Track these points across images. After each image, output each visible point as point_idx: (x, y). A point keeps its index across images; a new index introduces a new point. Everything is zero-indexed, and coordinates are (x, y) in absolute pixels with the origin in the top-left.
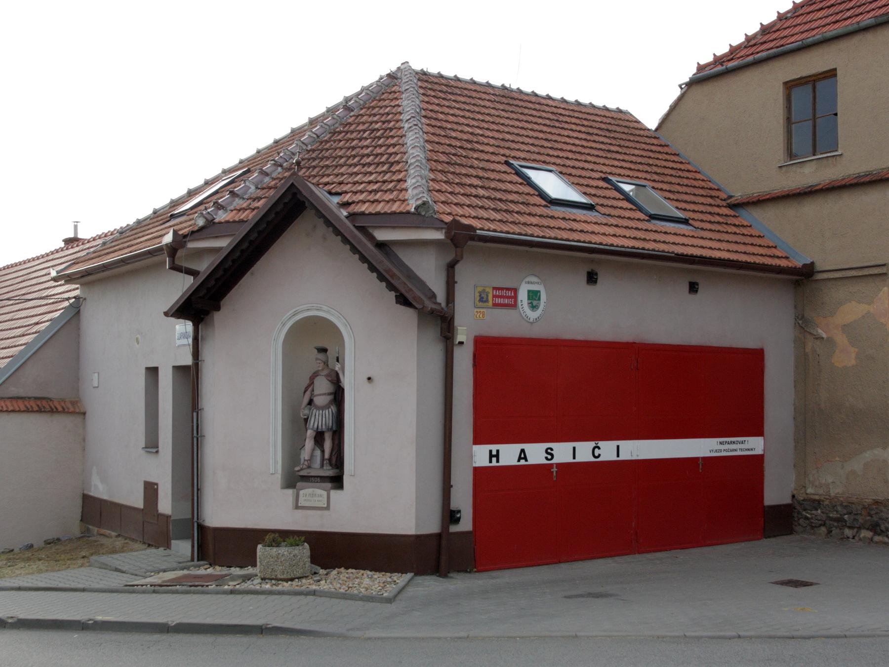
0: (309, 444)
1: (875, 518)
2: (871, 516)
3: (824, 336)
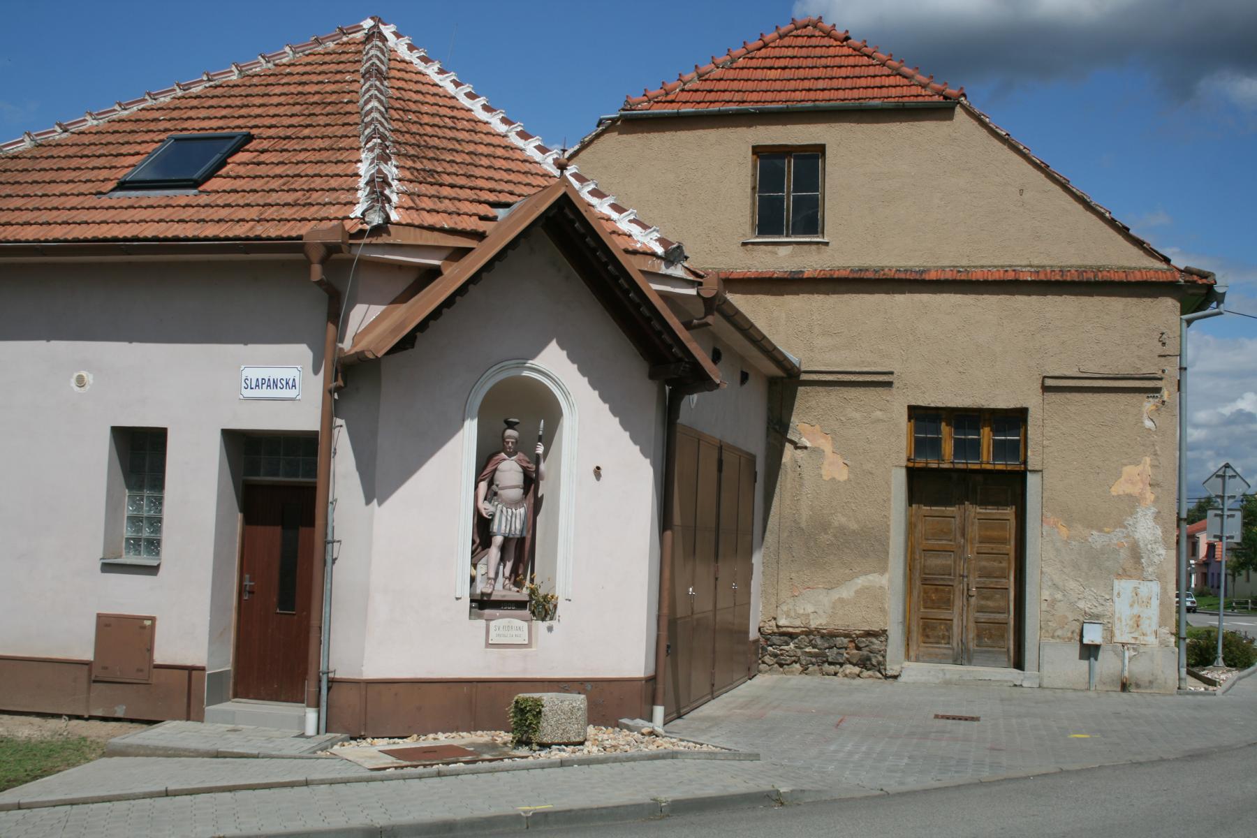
0: (494, 552)
1: (865, 652)
2: (858, 648)
3: (808, 444)
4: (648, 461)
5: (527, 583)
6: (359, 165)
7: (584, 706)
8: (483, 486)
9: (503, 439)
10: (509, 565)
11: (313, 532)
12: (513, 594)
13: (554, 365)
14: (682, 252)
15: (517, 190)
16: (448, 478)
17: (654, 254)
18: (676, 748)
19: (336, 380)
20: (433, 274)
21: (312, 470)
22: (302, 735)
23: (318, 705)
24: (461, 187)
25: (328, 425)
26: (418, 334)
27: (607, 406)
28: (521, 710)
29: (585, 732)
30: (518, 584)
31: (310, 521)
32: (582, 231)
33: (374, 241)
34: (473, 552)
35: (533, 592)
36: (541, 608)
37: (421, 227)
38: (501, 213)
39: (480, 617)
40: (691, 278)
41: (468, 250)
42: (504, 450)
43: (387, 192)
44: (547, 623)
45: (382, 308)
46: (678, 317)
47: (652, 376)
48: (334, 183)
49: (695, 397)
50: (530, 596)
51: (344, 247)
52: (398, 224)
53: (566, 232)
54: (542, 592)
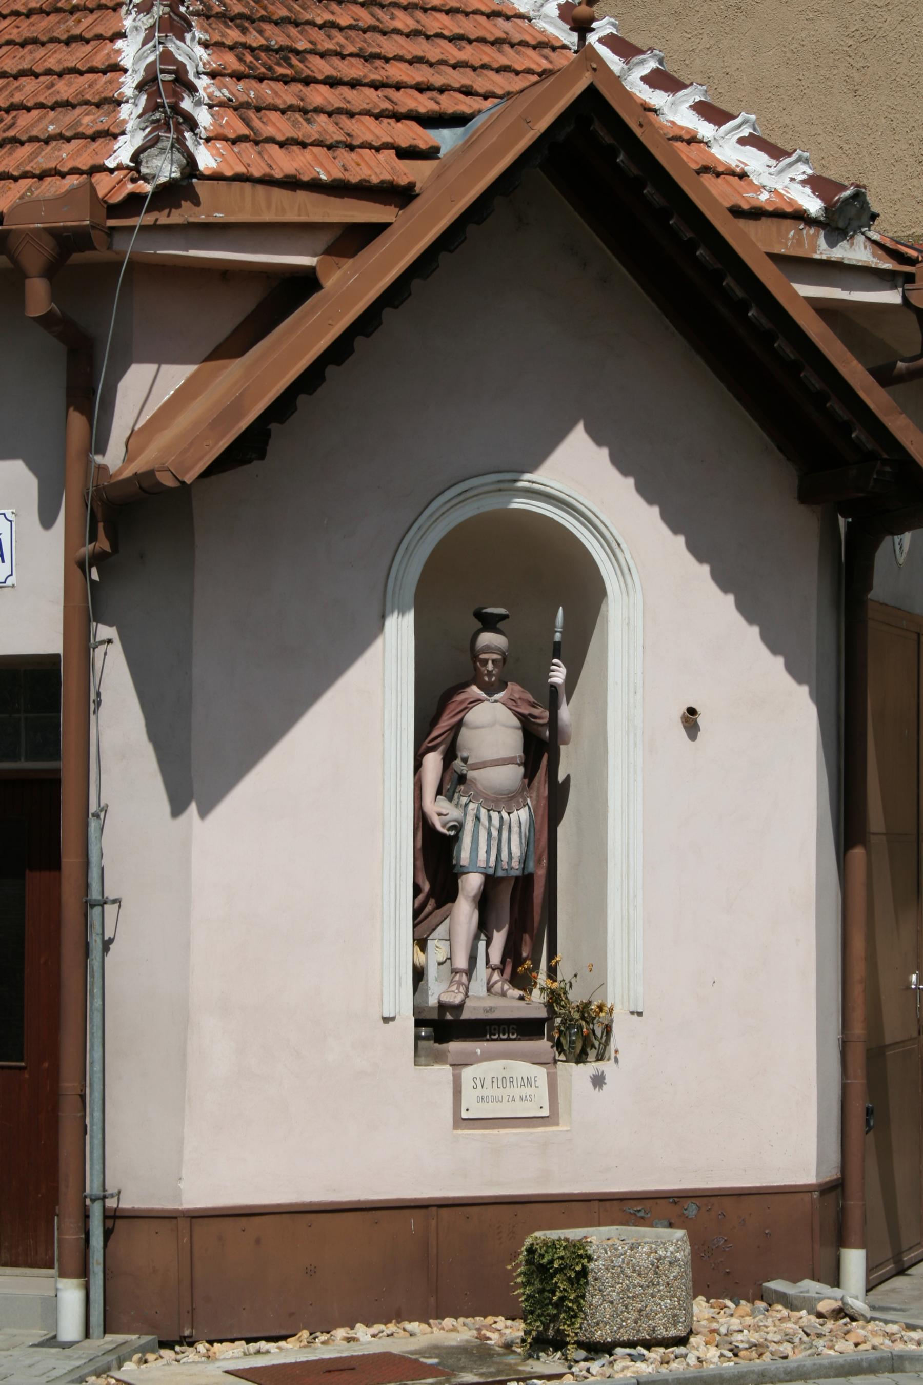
0: (464, 913)
4: (804, 690)
5: (542, 978)
6: (119, 44)
7: (683, 1254)
8: (433, 761)
9: (474, 654)
10: (499, 938)
11: (58, 883)
12: (511, 1005)
13: (581, 480)
14: (865, 205)
15: (481, 83)
16: (354, 745)
17: (800, 216)
18: (899, 1347)
19: (93, 538)
20: (302, 284)
21: (48, 741)
22: (52, 1342)
23: (84, 1272)
24: (354, 84)
25: (80, 642)
26: (274, 427)
27: (706, 569)
28: (540, 1269)
29: (689, 1313)
30: (522, 981)
31: (48, 855)
32: (634, 171)
33: (163, 218)
34: (416, 913)
35: (555, 998)
36: (577, 1033)
37: (267, 181)
38: (446, 139)
39: (439, 1058)
40: (888, 265)
41: (375, 230)
42: (476, 679)
43: (186, 104)
44: (590, 1068)
45: (189, 370)
46: (860, 358)
47: (806, 496)
48: (65, 89)
49: (907, 537)
50: (549, 1006)
51: (97, 237)
52: (216, 177)
53: (598, 178)
54: (576, 997)
